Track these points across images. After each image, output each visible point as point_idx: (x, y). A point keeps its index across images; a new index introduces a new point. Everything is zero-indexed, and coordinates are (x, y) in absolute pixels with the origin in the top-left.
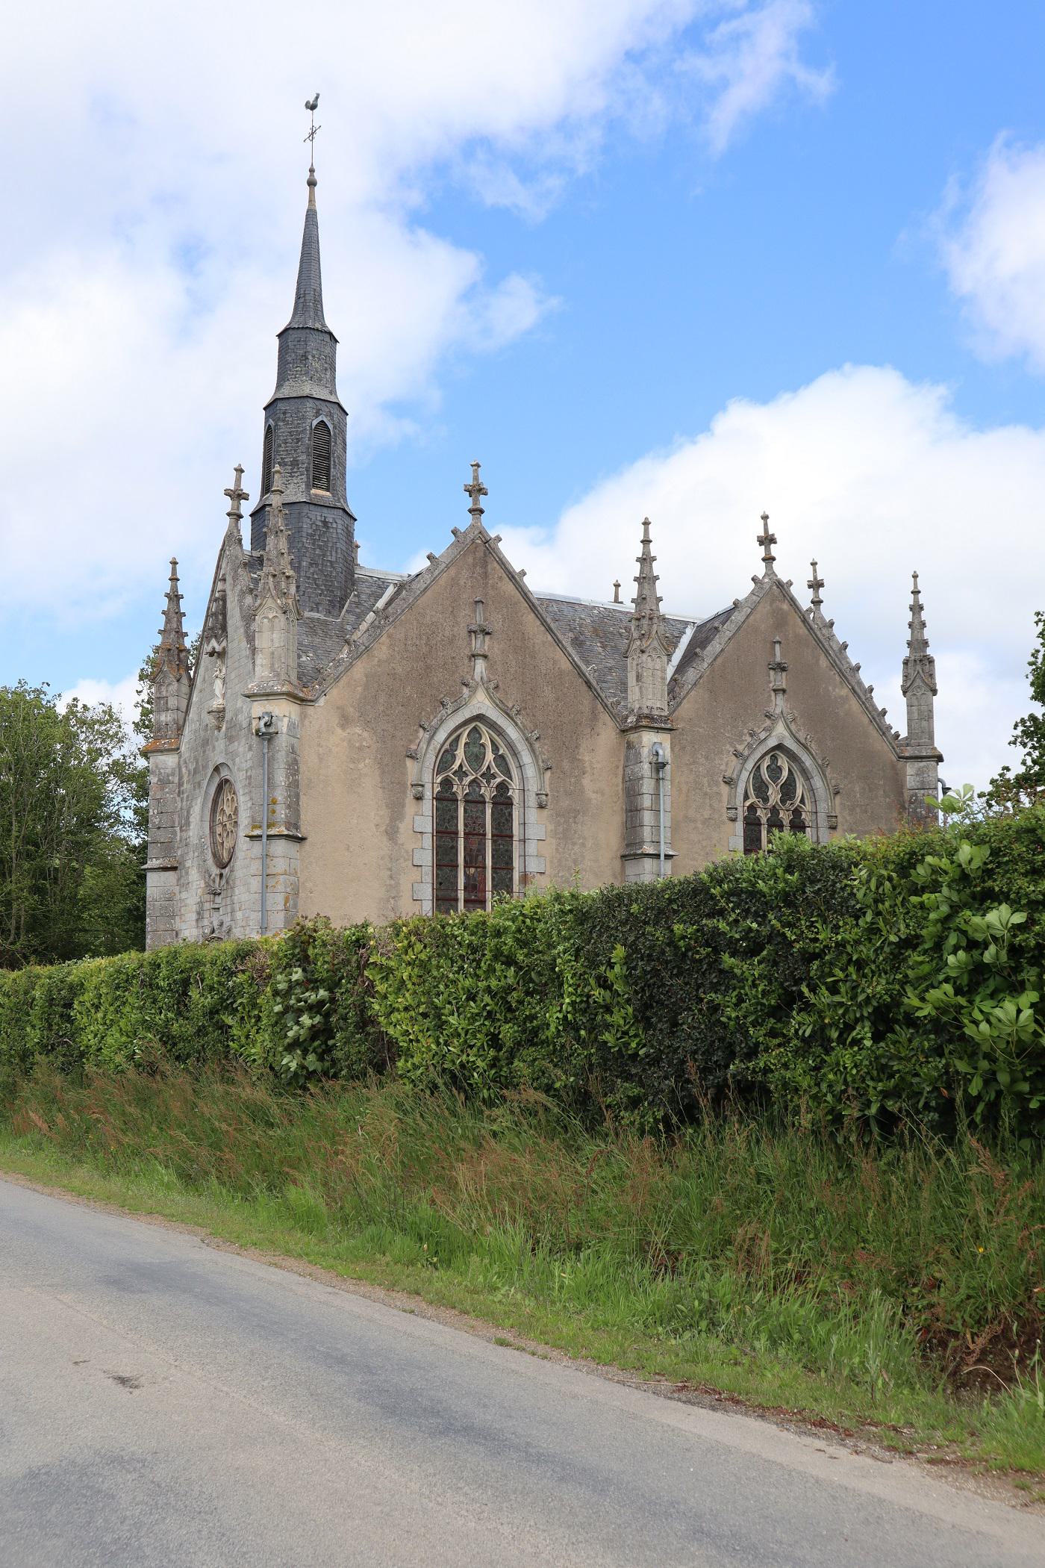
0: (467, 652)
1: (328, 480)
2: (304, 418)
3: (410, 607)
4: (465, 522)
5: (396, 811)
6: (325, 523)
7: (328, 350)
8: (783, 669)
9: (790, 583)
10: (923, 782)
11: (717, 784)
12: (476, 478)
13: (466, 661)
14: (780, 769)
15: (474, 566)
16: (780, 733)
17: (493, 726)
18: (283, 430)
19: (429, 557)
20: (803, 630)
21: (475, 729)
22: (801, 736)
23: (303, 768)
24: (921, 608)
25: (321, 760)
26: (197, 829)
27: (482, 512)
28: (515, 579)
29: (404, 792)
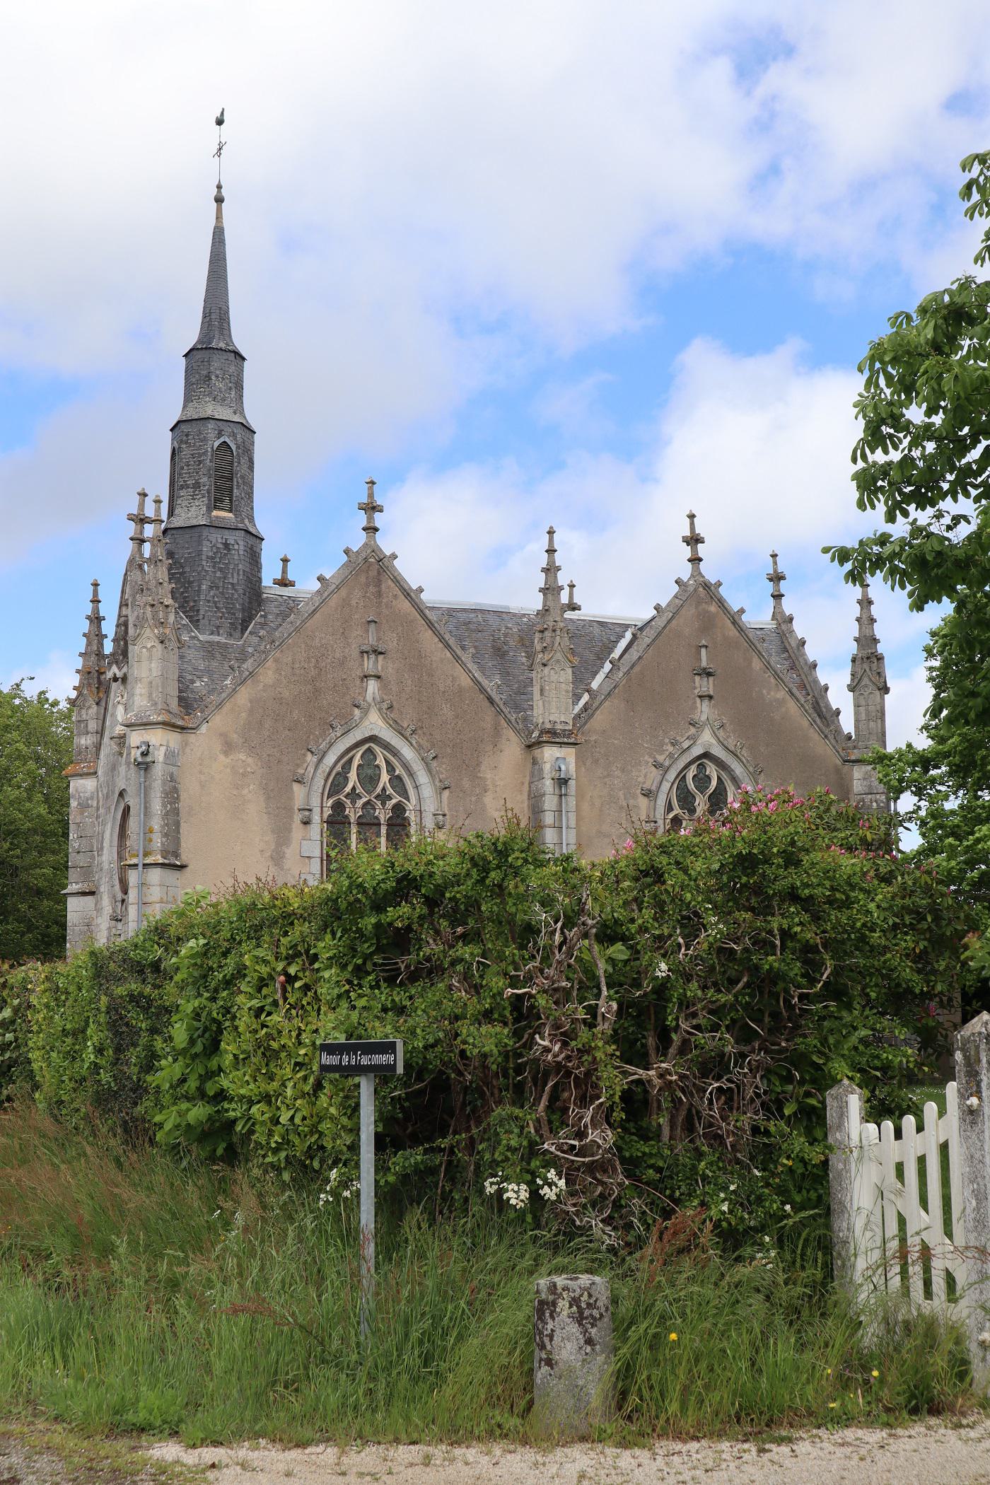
0: (359, 673)
1: (231, 500)
2: (205, 440)
3: (297, 630)
4: (357, 540)
5: (282, 835)
6: (226, 545)
7: (232, 369)
8: (709, 674)
9: (719, 584)
10: (870, 786)
11: (634, 797)
12: (371, 495)
13: (358, 682)
14: (709, 778)
15: (368, 585)
16: (706, 740)
17: (386, 746)
18: (186, 452)
19: (318, 579)
20: (733, 632)
21: (369, 749)
22: (731, 744)
23: (183, 796)
24: (870, 603)
25: (202, 786)
26: (108, 856)
27: (376, 530)
28: (411, 595)
29: (291, 817)
